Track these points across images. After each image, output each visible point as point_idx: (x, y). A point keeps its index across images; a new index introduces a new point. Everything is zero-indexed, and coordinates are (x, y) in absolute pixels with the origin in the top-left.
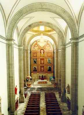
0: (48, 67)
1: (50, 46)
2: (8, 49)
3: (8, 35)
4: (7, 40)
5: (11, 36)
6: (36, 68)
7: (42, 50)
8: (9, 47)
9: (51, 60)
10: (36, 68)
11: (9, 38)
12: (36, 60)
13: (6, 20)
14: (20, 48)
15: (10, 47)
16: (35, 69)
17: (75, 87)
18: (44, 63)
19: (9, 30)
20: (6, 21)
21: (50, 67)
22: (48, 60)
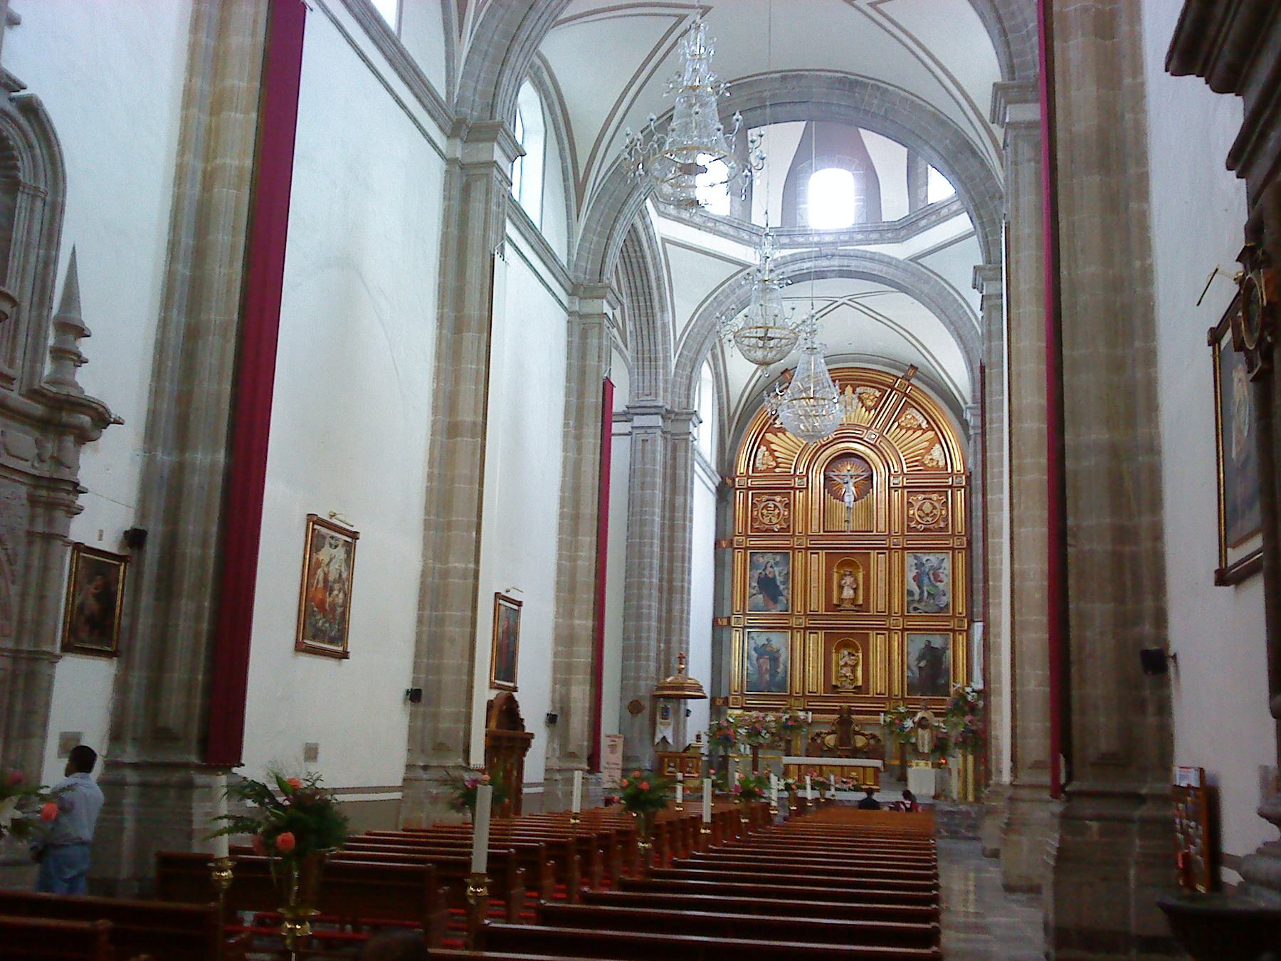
0: (917, 644)
1: (933, 425)
2: (456, 204)
3: (469, 94)
4: (457, 128)
5: (493, 107)
6: (774, 659)
7: (848, 468)
8: (466, 190)
9: (947, 564)
10: (784, 655)
11: (473, 114)
12: (777, 572)
13: (675, 338)
14: (591, 306)
15: (478, 193)
16: (767, 665)
17: (440, 622)
18: (864, 607)
19: (477, 58)
20: (675, 343)
21: (937, 641)
22: (911, 574)
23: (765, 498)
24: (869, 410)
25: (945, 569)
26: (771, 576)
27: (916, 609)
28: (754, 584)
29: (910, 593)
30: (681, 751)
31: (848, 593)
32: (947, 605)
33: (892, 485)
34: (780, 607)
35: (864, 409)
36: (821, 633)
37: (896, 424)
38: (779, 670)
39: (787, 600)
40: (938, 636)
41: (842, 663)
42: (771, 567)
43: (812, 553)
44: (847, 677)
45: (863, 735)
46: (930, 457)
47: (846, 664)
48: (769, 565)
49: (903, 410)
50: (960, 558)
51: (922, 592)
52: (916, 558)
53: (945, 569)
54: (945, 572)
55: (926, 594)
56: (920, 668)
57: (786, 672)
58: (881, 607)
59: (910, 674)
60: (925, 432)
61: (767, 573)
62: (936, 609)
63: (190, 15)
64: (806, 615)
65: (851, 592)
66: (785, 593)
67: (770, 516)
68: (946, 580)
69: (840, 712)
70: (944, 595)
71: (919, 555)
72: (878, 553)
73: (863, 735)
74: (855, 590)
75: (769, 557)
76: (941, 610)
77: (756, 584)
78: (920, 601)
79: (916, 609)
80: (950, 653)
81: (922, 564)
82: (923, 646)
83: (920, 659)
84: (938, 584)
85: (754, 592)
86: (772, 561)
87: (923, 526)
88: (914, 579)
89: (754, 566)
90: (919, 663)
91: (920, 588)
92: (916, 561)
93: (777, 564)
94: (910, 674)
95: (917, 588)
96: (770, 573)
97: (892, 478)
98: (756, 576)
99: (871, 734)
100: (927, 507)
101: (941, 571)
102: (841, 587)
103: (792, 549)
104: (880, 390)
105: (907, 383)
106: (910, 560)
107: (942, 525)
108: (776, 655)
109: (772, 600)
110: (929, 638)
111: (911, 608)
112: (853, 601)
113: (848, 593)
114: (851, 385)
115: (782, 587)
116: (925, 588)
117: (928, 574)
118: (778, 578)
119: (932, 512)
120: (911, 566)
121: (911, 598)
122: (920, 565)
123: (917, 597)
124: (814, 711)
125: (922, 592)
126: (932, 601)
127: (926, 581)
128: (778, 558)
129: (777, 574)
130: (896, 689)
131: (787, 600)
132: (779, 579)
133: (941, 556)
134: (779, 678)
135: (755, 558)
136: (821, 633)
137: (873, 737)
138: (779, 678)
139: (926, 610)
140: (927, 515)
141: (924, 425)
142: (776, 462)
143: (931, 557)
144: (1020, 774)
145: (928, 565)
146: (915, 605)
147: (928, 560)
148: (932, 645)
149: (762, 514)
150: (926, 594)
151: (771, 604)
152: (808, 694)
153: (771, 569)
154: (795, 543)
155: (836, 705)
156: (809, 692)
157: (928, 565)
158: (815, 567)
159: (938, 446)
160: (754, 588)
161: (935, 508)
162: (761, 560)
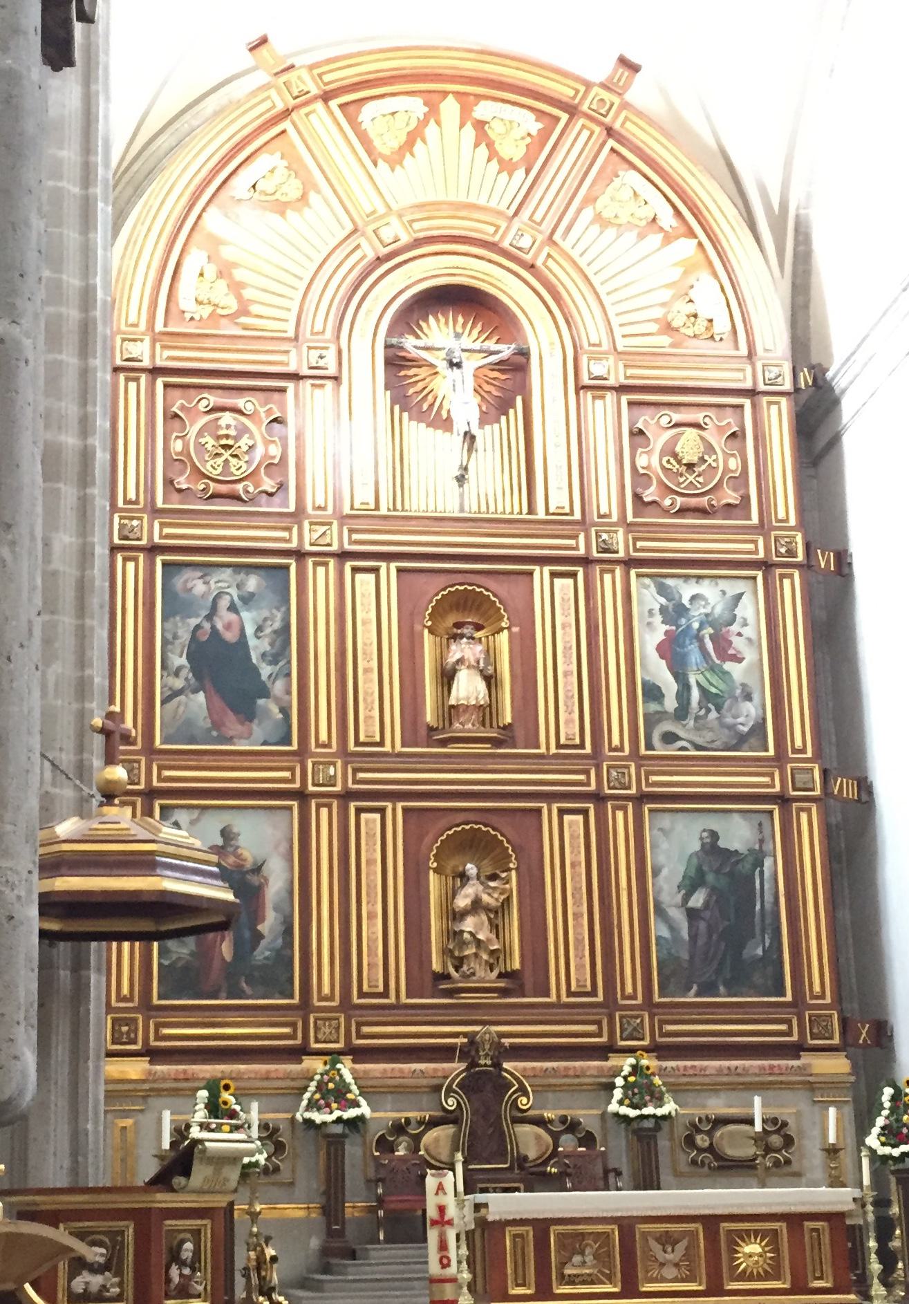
9: (751, 610)
10: (277, 880)
22: (651, 636)
23: (213, 399)
24: (507, 167)
25: (745, 624)
26: (231, 636)
27: (669, 738)
28: (179, 660)
29: (653, 693)
30: (148, 1169)
31: (468, 688)
32: (760, 726)
33: (586, 380)
34: (258, 730)
35: (494, 165)
36: (396, 811)
37: (588, 214)
38: (264, 928)
39: (285, 711)
40: (736, 816)
41: (462, 902)
42: (233, 608)
43: (355, 570)
44: (479, 943)
45: (540, 1122)
46: (690, 309)
47: (476, 906)
48: (224, 603)
49: (608, 176)
50: (791, 590)
51: (684, 688)
52: (662, 590)
53: (745, 624)
54: (748, 632)
55: (695, 694)
56: (692, 914)
57: (289, 931)
58: (569, 730)
59: (665, 933)
60: (668, 239)
61: (219, 626)
62: (724, 736)
63: (76, 395)
64: (344, 752)
65: (481, 686)
66: (278, 687)
67: (226, 455)
68: (749, 656)
69: (469, 1052)
70: (748, 697)
71: (670, 582)
72: (554, 575)
73: (540, 1122)
74: (491, 680)
75: (223, 581)
76: (741, 741)
77: (183, 661)
78: (682, 713)
79: (669, 738)
80: (774, 865)
81: (681, 610)
82: (697, 846)
83: (691, 884)
84: (728, 666)
85: (179, 683)
86: (234, 592)
87: (679, 500)
88: (662, 649)
89: (175, 605)
90: (686, 898)
91: (680, 677)
92: (663, 601)
93: (248, 599)
94: (665, 933)
95: (669, 677)
96: (228, 626)
97: (584, 360)
98: (185, 636)
99: (563, 1120)
100: (689, 444)
101: (735, 628)
102: (447, 677)
103: (300, 555)
104: (540, 114)
105: (617, 101)
106: (647, 596)
107: (731, 497)
108: (254, 880)
109: (235, 711)
110: (714, 823)
111: (656, 740)
112: (487, 712)
113: (468, 688)
114: (457, 94)
115: (266, 670)
116: (692, 680)
117: (700, 640)
118: (252, 642)
119: (703, 460)
120: (651, 612)
121: (654, 707)
122: (675, 612)
123: (670, 704)
124: (360, 1054)
125: (684, 688)
126: (713, 715)
127: (695, 657)
128: (253, 583)
129: (250, 630)
130: (630, 981)
131: (285, 711)
132: (258, 647)
133: (733, 588)
134: (262, 953)
135: (179, 582)
136: (396, 811)
137: (572, 1126)
138: (262, 953)
139: (699, 741)
140: (690, 466)
141: (667, 219)
142: (239, 298)
143: (708, 590)
144: (171, 323)
145: (697, 612)
146: (668, 726)
147: (694, 598)
148: (722, 843)
149: (201, 447)
150: (695, 694)
151: (233, 725)
152: (356, 1000)
153: (232, 617)
154: (309, 537)
155: (453, 1033)
156: (362, 994)
157: (697, 612)
158: (366, 613)
159: (705, 276)
160: (177, 674)
161: (710, 449)
162: (199, 588)
